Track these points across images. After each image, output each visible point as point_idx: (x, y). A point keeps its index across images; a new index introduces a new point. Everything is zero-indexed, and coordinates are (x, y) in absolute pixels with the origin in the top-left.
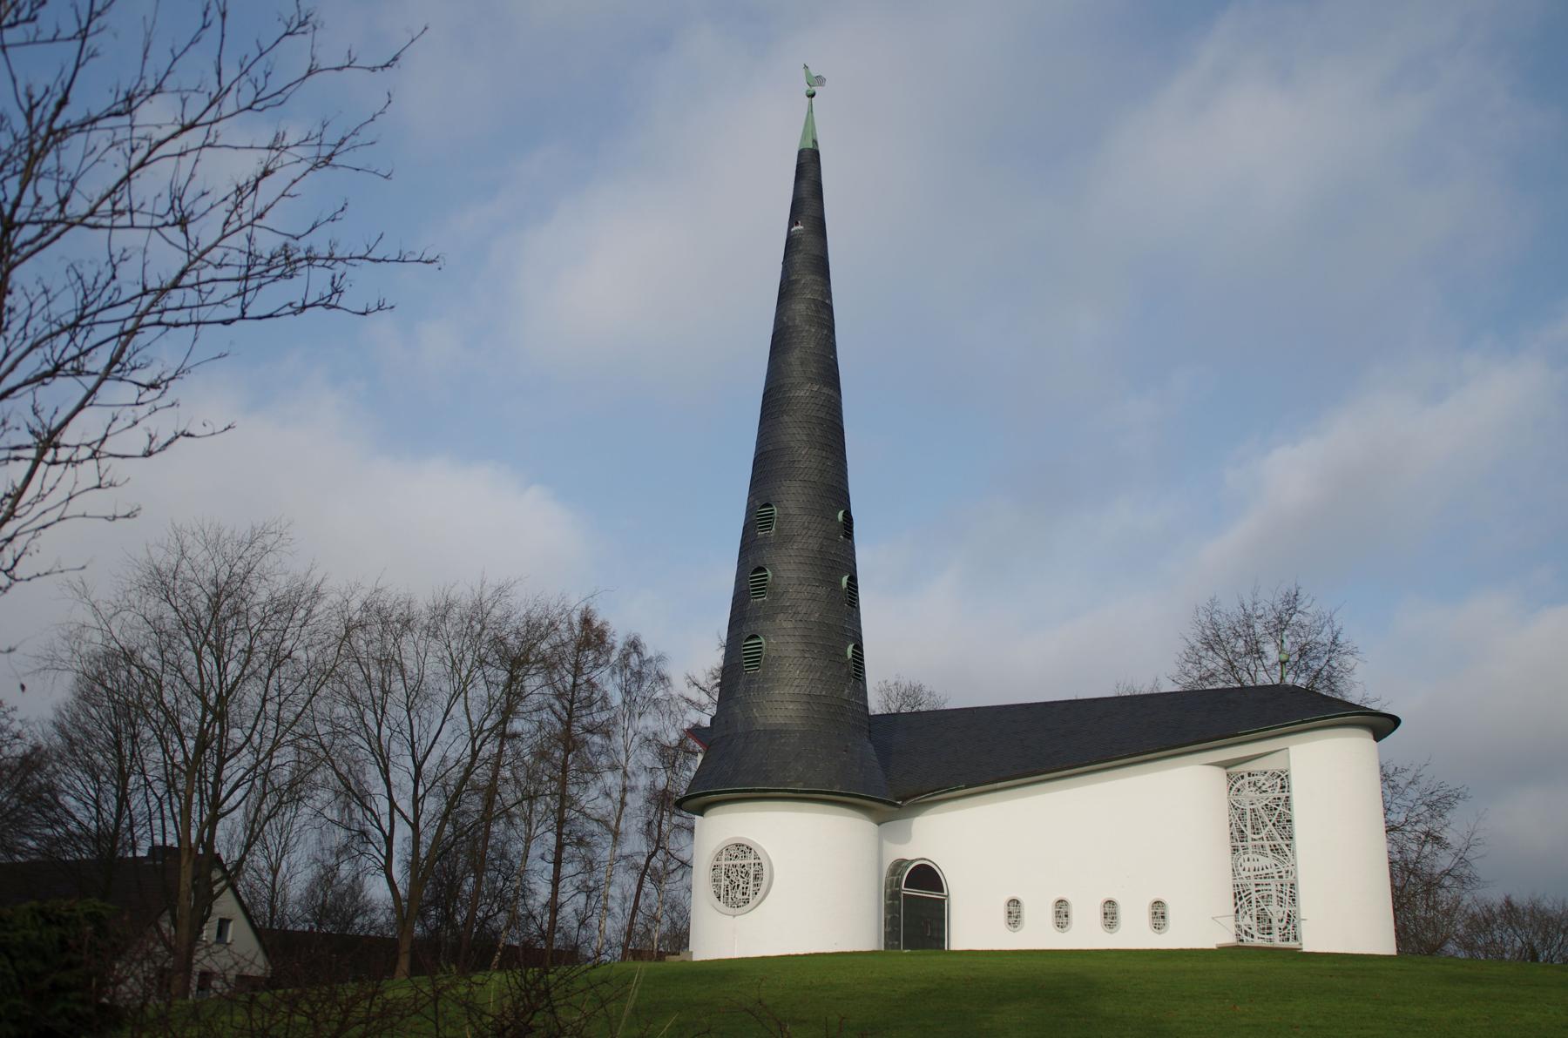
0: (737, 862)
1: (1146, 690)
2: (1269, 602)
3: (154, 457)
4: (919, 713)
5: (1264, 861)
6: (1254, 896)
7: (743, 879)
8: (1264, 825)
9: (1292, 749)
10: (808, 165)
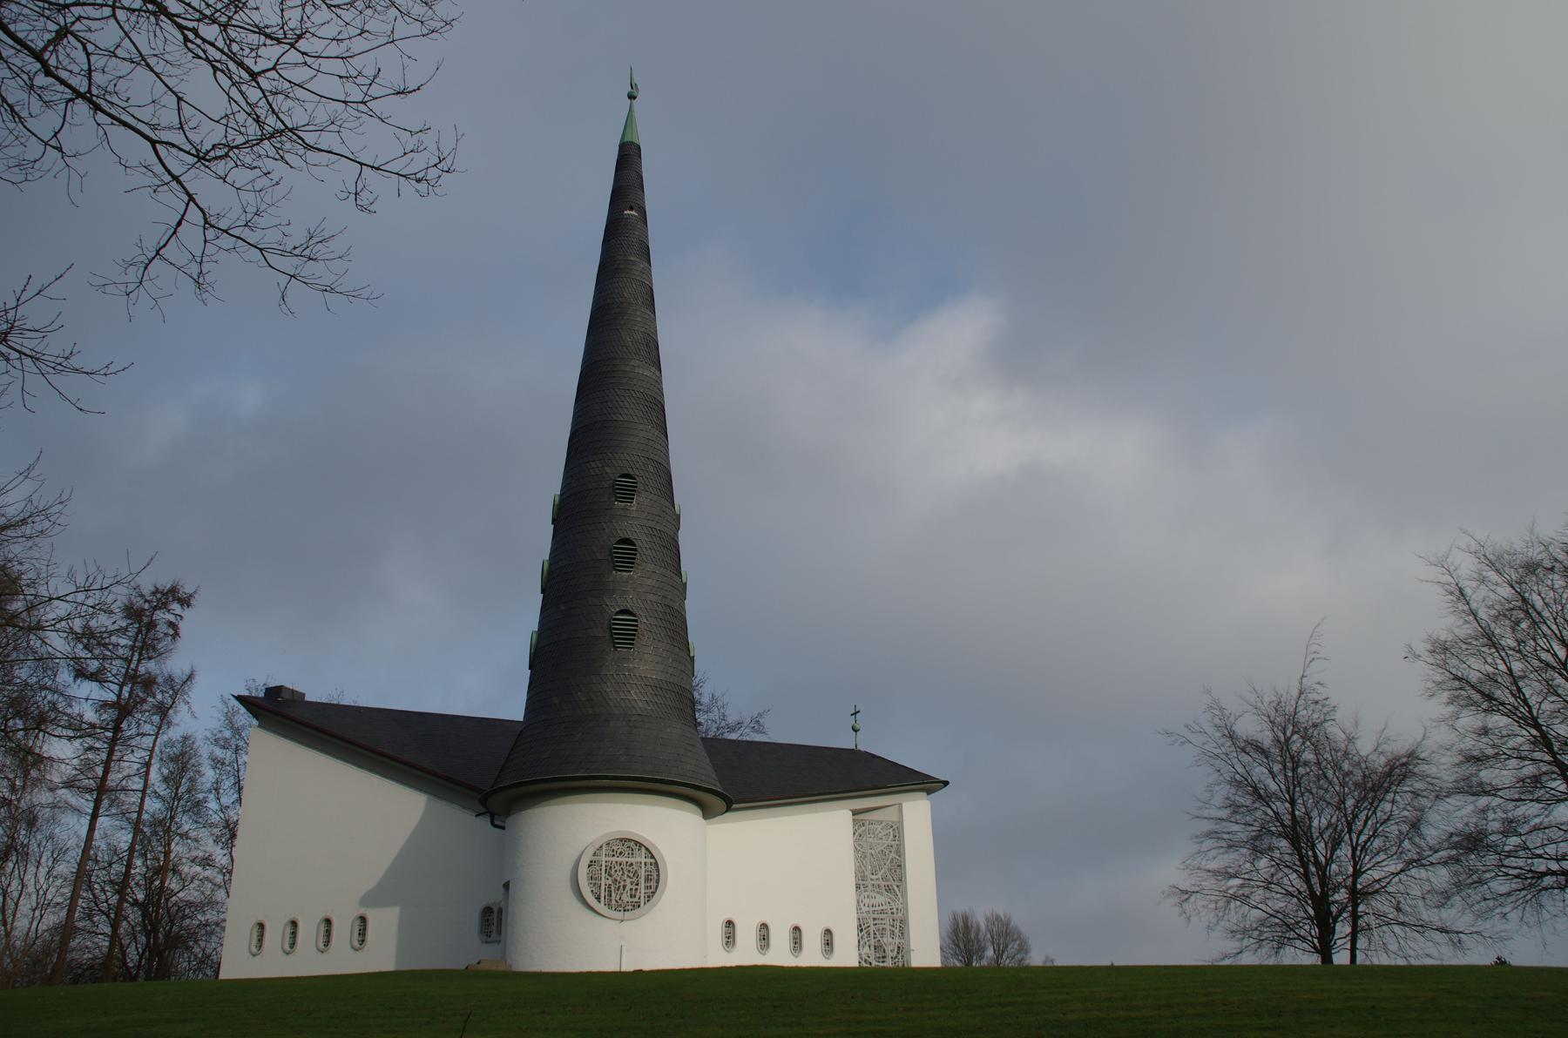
0: (623, 859)
1: (324, 701)
5: (880, 899)
6: (872, 928)
7: (628, 879)
9: (905, 805)
10: (628, 157)
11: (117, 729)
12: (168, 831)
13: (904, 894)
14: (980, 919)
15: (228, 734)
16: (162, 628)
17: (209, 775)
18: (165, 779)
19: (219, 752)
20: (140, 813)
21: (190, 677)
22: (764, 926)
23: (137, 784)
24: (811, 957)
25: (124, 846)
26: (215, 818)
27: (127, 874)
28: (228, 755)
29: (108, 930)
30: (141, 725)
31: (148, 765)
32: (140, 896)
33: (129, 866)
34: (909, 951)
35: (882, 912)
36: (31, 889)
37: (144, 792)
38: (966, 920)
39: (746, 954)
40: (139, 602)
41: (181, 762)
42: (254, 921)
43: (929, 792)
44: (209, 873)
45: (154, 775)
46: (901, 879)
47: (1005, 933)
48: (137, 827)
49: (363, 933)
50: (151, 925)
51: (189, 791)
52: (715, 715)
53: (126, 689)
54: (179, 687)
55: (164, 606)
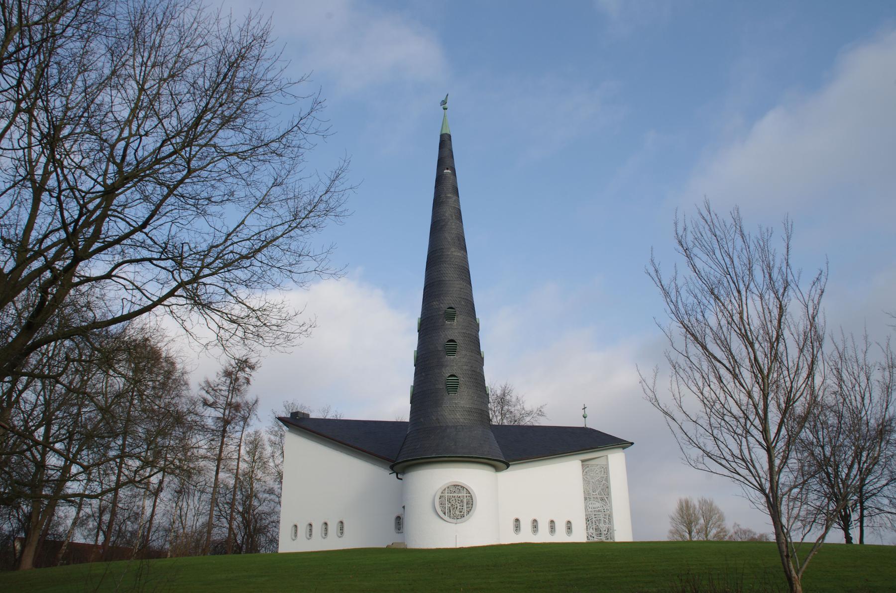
0: (455, 495)
2: (244, 358)
3: (826, 290)
4: (519, 426)
5: (597, 505)
7: (458, 504)
8: (598, 491)
10: (445, 142)
11: (224, 431)
12: (251, 478)
13: (610, 502)
14: (695, 502)
15: (276, 429)
16: (242, 380)
17: (268, 450)
18: (248, 453)
19: (273, 438)
20: (237, 469)
21: (256, 401)
22: (535, 521)
23: (235, 456)
24: (561, 537)
25: (231, 486)
26: (273, 471)
27: (234, 499)
28: (277, 439)
29: (228, 526)
30: (236, 433)
31: (239, 446)
32: (241, 509)
33: (234, 495)
34: (614, 530)
35: (599, 511)
36: (192, 507)
37: (238, 459)
38: (687, 502)
39: (526, 537)
40: (231, 369)
41: (255, 445)
42: (292, 524)
43: (624, 448)
44: (273, 497)
45: (243, 452)
46: (609, 494)
47: (710, 511)
48: (237, 478)
49: (342, 529)
50: (246, 523)
51: (260, 458)
52: (518, 407)
53: (227, 412)
54: (251, 407)
55: (242, 369)
